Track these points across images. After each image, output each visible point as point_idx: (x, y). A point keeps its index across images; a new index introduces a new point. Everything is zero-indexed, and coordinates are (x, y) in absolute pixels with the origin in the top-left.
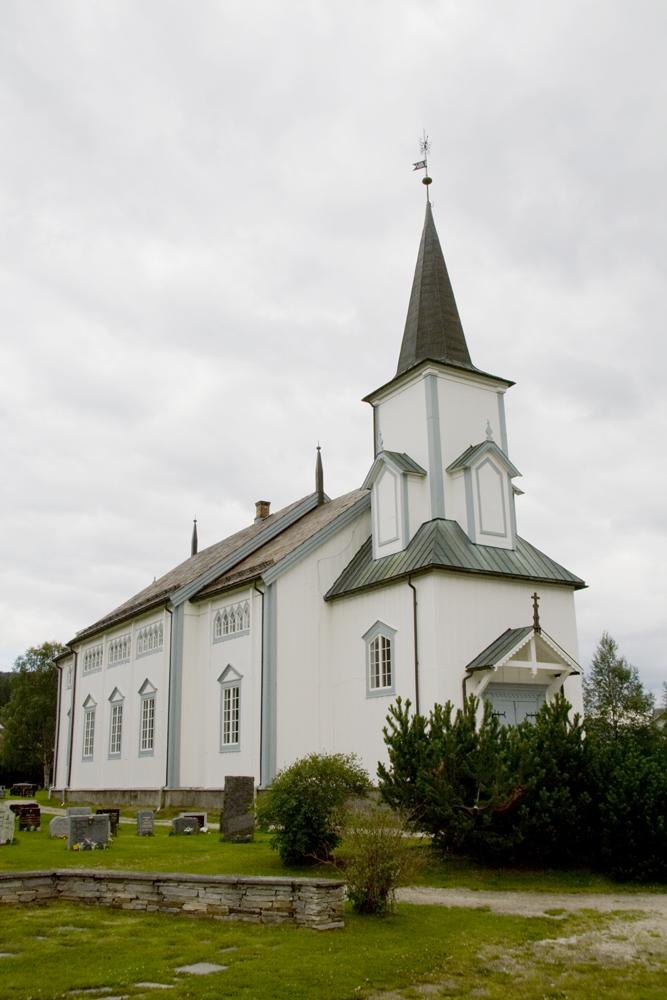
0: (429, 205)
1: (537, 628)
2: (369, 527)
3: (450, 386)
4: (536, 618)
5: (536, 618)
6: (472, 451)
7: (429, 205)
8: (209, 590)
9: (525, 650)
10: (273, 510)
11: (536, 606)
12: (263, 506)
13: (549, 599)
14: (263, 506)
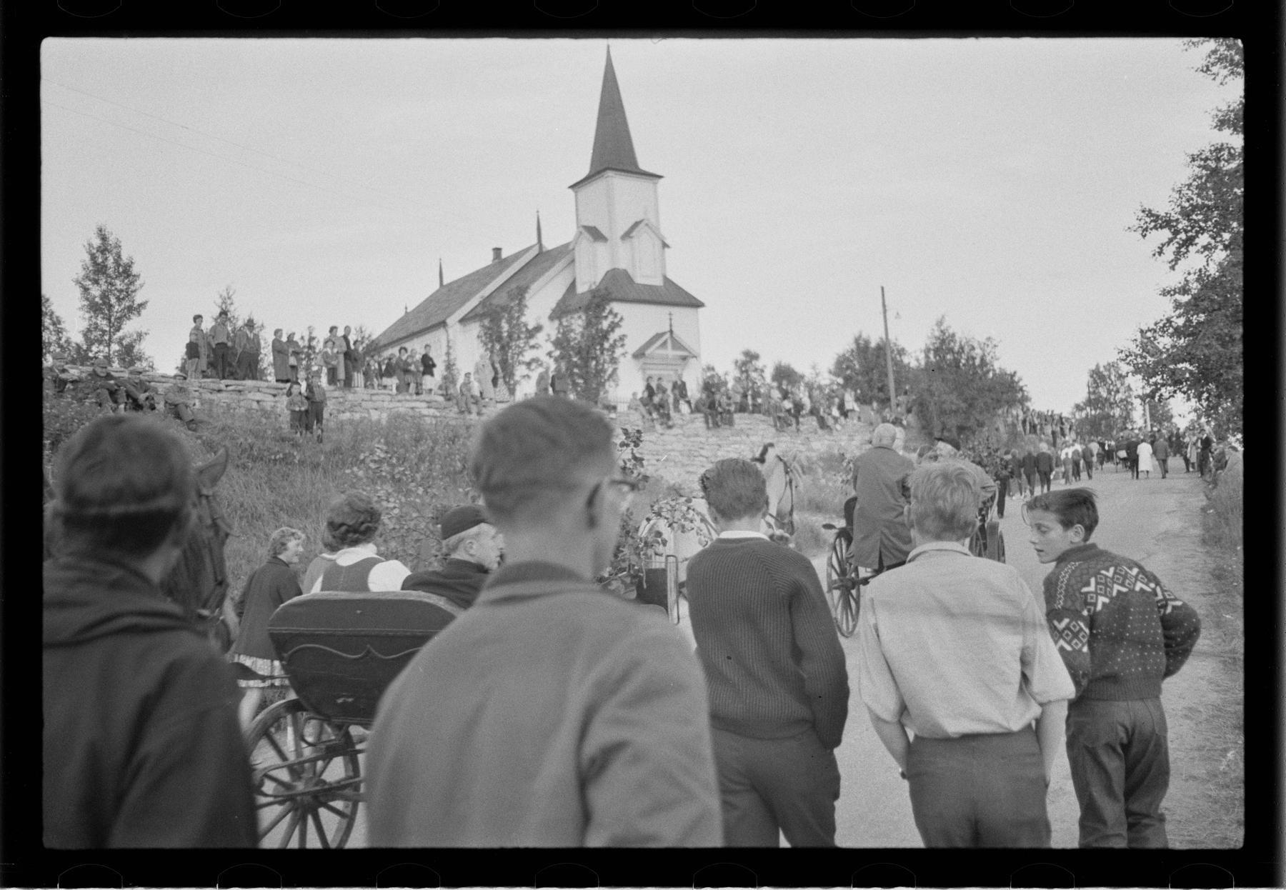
1: (671, 332)
2: (574, 272)
3: (618, 183)
4: (671, 326)
5: (671, 326)
6: (636, 224)
8: (89, 635)
9: (665, 343)
10: (504, 255)
11: (671, 319)
12: (497, 251)
13: (681, 315)
14: (497, 251)
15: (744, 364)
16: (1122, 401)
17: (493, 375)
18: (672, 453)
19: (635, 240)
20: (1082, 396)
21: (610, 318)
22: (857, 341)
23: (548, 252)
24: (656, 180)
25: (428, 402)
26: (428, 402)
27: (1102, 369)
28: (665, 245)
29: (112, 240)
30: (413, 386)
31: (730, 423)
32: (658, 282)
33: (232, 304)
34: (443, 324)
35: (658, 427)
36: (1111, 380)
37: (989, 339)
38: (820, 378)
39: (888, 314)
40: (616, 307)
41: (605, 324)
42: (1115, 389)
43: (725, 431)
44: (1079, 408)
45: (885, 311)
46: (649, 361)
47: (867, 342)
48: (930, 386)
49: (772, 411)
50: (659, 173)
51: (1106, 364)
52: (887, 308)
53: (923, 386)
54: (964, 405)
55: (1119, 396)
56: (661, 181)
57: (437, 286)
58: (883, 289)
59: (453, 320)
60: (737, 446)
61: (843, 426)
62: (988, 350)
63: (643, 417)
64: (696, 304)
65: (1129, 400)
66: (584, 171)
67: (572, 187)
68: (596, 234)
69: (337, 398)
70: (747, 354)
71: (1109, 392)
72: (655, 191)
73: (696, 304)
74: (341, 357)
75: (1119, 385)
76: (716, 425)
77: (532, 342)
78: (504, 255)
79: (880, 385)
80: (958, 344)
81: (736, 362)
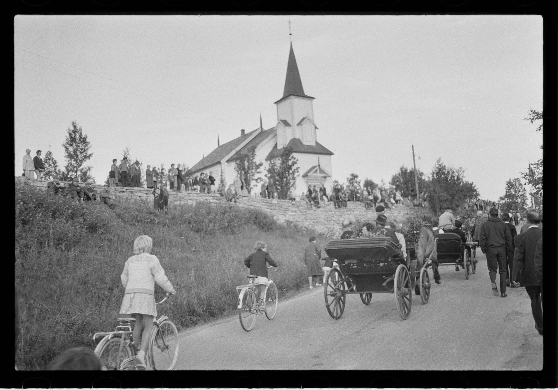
0: (291, 42)
1: (319, 166)
2: (276, 140)
3: (296, 101)
4: (319, 163)
5: (319, 163)
7: (291, 42)
9: (316, 170)
10: (246, 132)
11: (319, 160)
12: (243, 131)
14: (243, 131)
15: (351, 179)
16: (521, 195)
17: (241, 184)
18: (320, 219)
19: (303, 126)
20: (503, 193)
21: (292, 160)
22: (401, 169)
23: (265, 131)
24: (312, 99)
25: (213, 197)
26: (213, 197)
27: (512, 181)
28: (316, 128)
29: (78, 127)
30: (206, 189)
31: (346, 206)
32: (313, 144)
33: (128, 154)
34: (219, 163)
35: (314, 208)
36: (516, 186)
37: (461, 168)
38: (385, 186)
39: (415, 157)
40: (295, 155)
41: (290, 163)
42: (518, 190)
43: (343, 209)
44: (502, 199)
45: (414, 156)
46: (309, 178)
47: (406, 170)
48: (434, 189)
49: (364, 200)
50: (313, 97)
51: (514, 179)
52: (415, 155)
53: (432, 189)
54: (450, 198)
55: (520, 193)
56: (314, 100)
57: (217, 146)
58: (413, 146)
59: (223, 161)
60: (349, 216)
61: (396, 207)
62: (460, 173)
63: (307, 203)
64: (330, 154)
65: (525, 195)
66: (281, 96)
67: (276, 103)
68: (286, 123)
69: (174, 195)
70: (353, 175)
71: (515, 192)
72: (312, 105)
73: (330, 154)
74: (176, 177)
75: (520, 188)
76: (339, 207)
77: (258, 170)
78: (246, 132)
79: (412, 189)
80: (447, 171)
81: (348, 179)
